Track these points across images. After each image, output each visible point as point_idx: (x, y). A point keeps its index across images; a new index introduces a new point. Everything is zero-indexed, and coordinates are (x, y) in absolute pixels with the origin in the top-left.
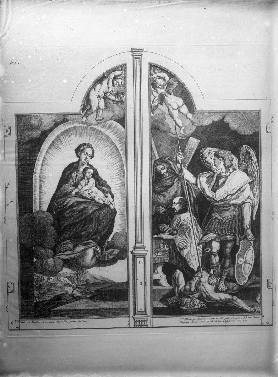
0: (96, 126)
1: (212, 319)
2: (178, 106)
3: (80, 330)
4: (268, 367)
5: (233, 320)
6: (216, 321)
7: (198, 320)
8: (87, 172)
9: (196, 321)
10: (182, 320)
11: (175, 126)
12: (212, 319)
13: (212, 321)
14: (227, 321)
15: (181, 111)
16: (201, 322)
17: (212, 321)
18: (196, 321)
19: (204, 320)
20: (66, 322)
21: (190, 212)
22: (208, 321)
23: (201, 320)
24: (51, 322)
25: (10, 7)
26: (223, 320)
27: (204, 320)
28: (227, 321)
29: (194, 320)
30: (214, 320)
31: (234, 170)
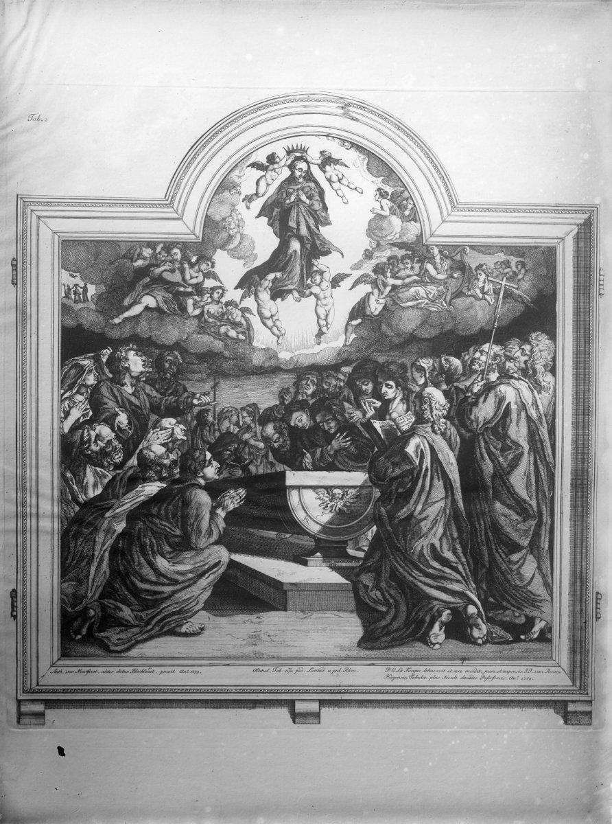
0: (253, 312)
1: (455, 672)
2: (278, 338)
3: (305, 115)
4: (591, 807)
5: (501, 675)
6: (464, 678)
7: (425, 674)
8: (431, 633)
9: (420, 675)
10: (389, 673)
11: (221, 283)
12: (455, 672)
13: (456, 678)
14: (489, 678)
15: (517, 560)
16: (431, 678)
17: (456, 678)
18: (420, 675)
19: (438, 675)
20: (153, 671)
21: (570, 686)
22: (446, 677)
23: (432, 674)
24: (120, 671)
25: (36, 18)
26: (479, 675)
27: (438, 675)
28: (489, 678)
29: (416, 674)
30: (460, 675)
31: (209, 275)
